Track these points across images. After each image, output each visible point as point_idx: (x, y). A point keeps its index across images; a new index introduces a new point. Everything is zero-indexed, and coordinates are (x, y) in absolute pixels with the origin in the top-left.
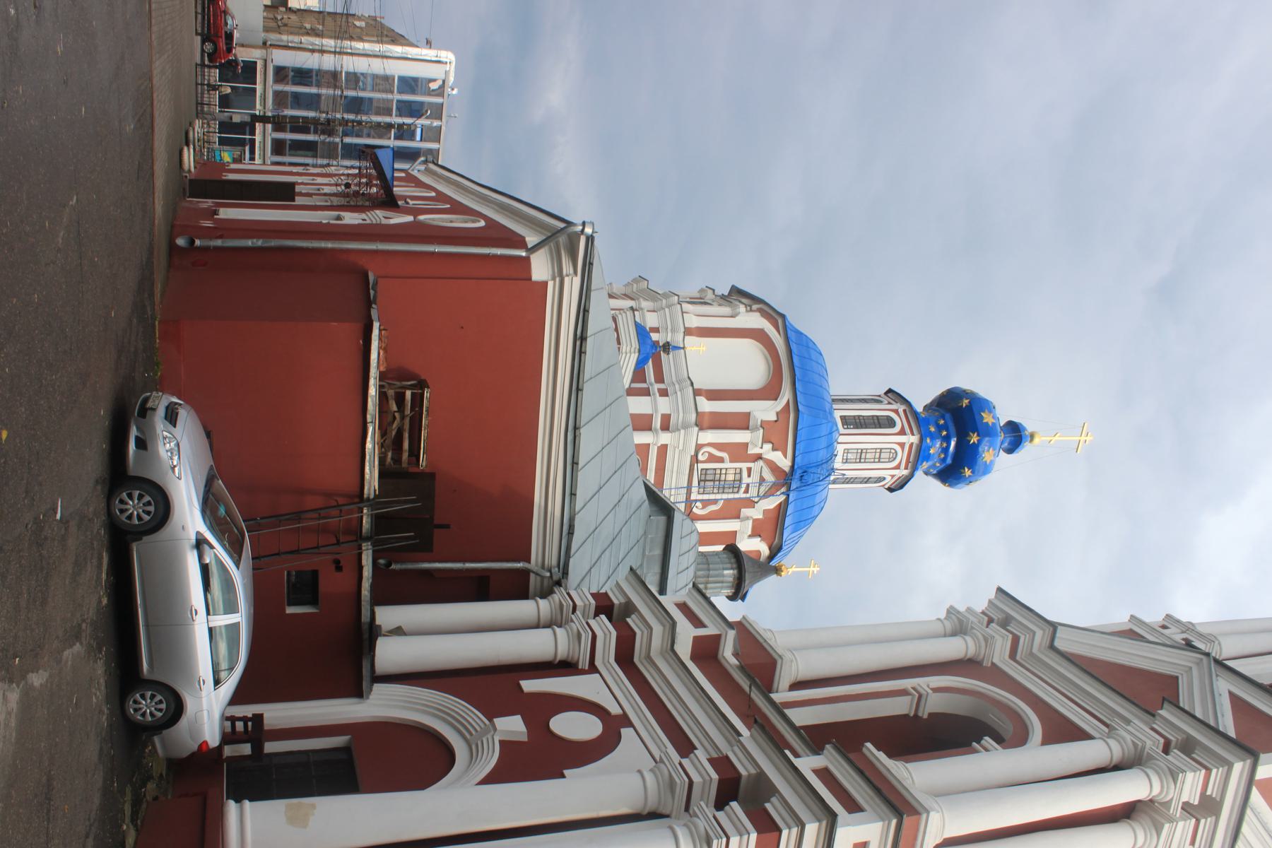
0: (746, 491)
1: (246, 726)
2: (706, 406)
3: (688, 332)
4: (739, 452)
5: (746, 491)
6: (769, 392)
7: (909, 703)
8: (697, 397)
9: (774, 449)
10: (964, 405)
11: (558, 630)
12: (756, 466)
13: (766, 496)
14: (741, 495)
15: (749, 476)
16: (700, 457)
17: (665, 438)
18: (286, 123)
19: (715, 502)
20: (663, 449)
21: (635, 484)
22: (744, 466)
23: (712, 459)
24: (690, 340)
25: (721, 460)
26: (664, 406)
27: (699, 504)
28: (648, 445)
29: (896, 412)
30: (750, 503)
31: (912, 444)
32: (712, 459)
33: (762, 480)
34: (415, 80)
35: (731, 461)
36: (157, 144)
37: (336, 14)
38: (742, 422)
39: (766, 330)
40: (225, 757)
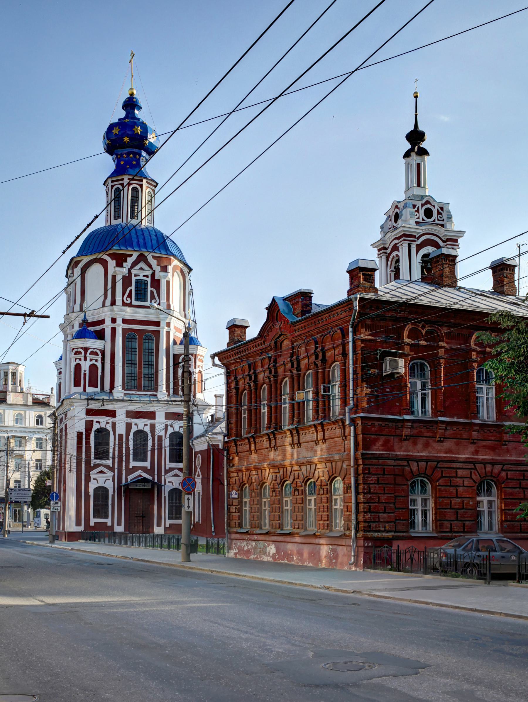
0: (147, 277)
2: (108, 302)
4: (127, 281)
5: (147, 277)
9: (126, 261)
11: (238, 378)
12: (134, 272)
13: (150, 266)
14: (149, 280)
15: (139, 276)
16: (129, 302)
17: (119, 321)
19: (152, 292)
20: (125, 321)
22: (134, 279)
23: (130, 296)
25: (131, 291)
26: (108, 322)
28: (123, 329)
30: (153, 275)
31: (147, 182)
33: (141, 269)
34: (390, 571)
35: (131, 286)
39: (195, 554)
40: (273, 561)
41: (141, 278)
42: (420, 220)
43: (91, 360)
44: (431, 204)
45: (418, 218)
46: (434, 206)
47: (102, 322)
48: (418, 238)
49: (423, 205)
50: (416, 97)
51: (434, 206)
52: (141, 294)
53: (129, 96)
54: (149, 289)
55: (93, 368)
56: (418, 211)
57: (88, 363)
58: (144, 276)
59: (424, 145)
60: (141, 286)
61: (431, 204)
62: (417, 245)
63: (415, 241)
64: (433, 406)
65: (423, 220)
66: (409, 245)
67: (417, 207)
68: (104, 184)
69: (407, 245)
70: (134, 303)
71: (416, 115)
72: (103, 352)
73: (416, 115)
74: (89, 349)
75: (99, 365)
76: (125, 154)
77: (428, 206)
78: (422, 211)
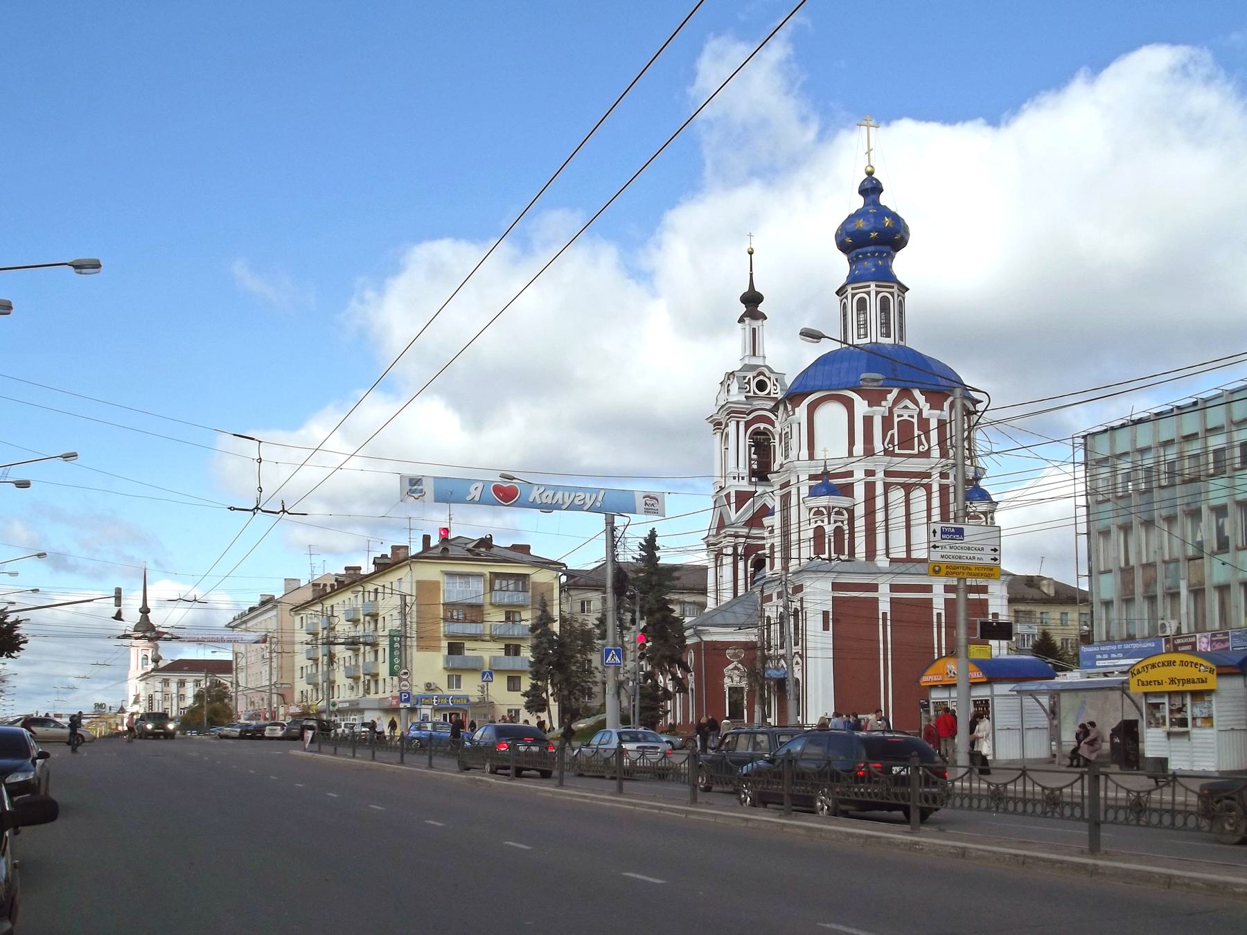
0: (912, 417)
1: (514, 618)
2: (859, 448)
3: (811, 457)
4: (887, 422)
5: (912, 417)
6: (849, 404)
7: (1073, 694)
8: (854, 455)
9: (886, 400)
10: (886, 219)
12: (896, 411)
13: (916, 403)
14: (915, 421)
15: (902, 416)
18: (715, 822)
21: (999, 694)
22: (896, 420)
23: (892, 441)
24: (819, 454)
25: (893, 435)
27: (921, 447)
29: (853, 296)
30: (921, 411)
32: (892, 441)
33: (906, 407)
36: (1172, 870)
37: (294, 678)
38: (868, 421)
41: (905, 417)
42: (751, 394)
43: (816, 522)
44: (765, 376)
45: (749, 392)
46: (769, 379)
47: (850, 474)
48: (748, 414)
49: (754, 378)
50: (751, 253)
51: (769, 379)
52: (906, 440)
53: (867, 176)
54: (916, 432)
55: (838, 532)
56: (749, 383)
57: (833, 526)
58: (909, 416)
59: (761, 308)
60: (905, 426)
61: (765, 376)
62: (746, 422)
63: (744, 418)
64: (186, 668)
65: (754, 393)
66: (738, 422)
67: (747, 378)
68: (837, 293)
69: (735, 422)
70: (897, 451)
71: (751, 275)
72: (851, 512)
73: (751, 275)
74: (834, 508)
75: (846, 527)
76: (870, 253)
77: (761, 377)
78: (753, 384)
